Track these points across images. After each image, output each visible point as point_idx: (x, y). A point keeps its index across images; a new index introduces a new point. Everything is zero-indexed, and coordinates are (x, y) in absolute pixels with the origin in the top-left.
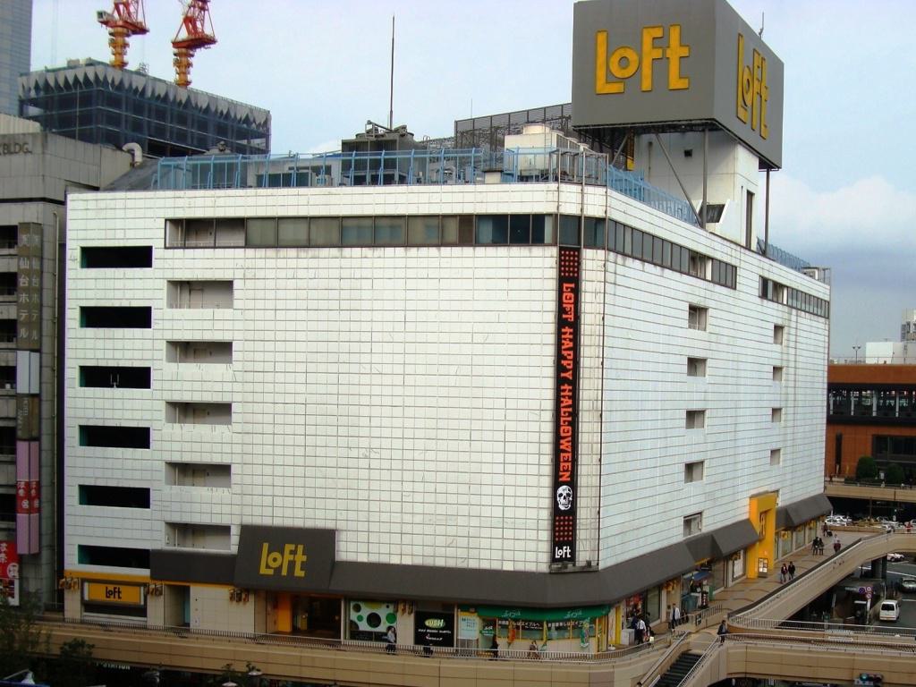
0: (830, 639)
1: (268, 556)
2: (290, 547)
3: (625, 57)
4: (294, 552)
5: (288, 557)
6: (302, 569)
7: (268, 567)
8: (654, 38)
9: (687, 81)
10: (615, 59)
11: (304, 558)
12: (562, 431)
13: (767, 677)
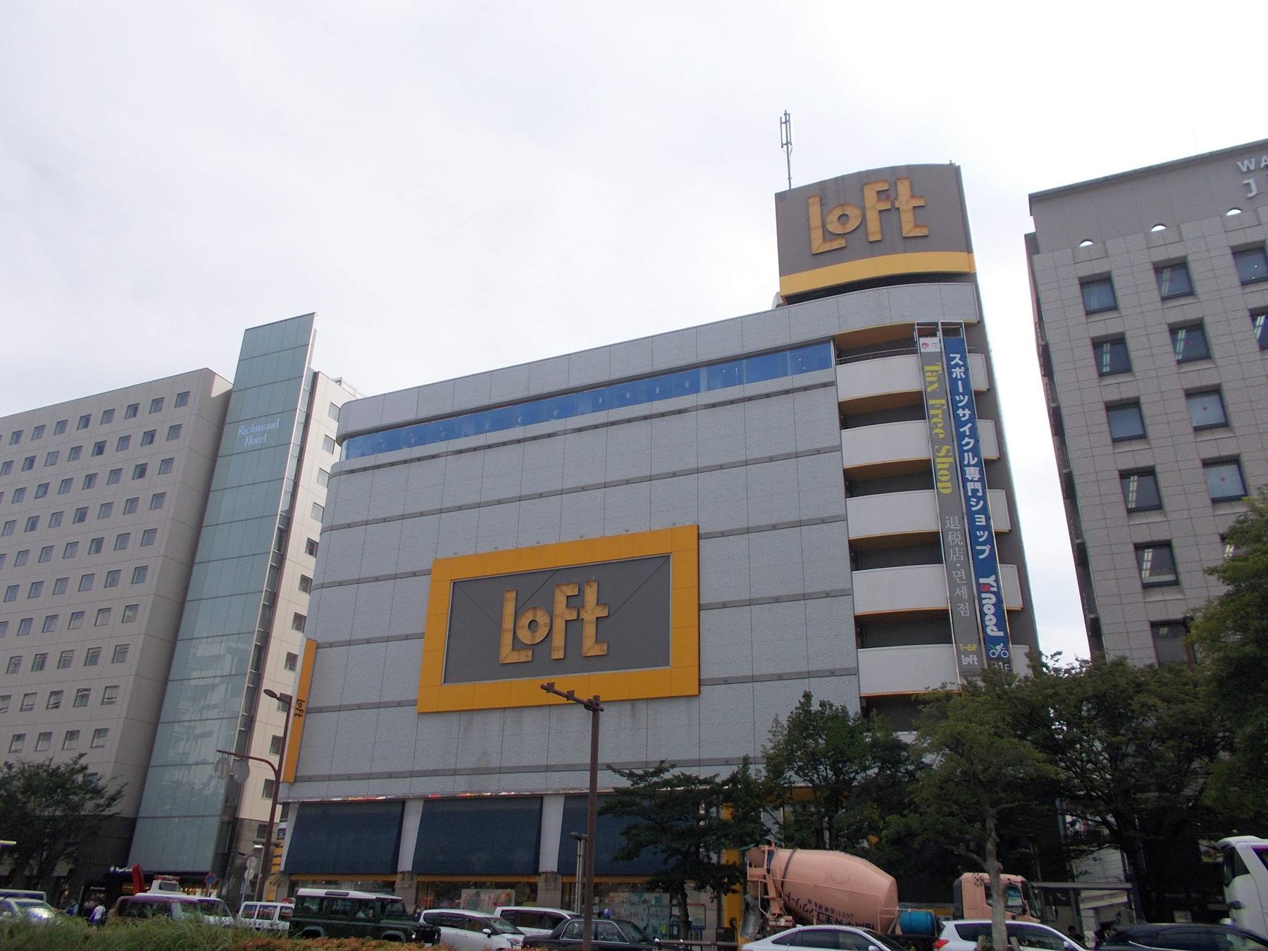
0: (171, 877)
2: (971, 656)
3: (847, 215)
4: (973, 657)
8: (880, 211)
9: (605, 647)
10: (525, 621)
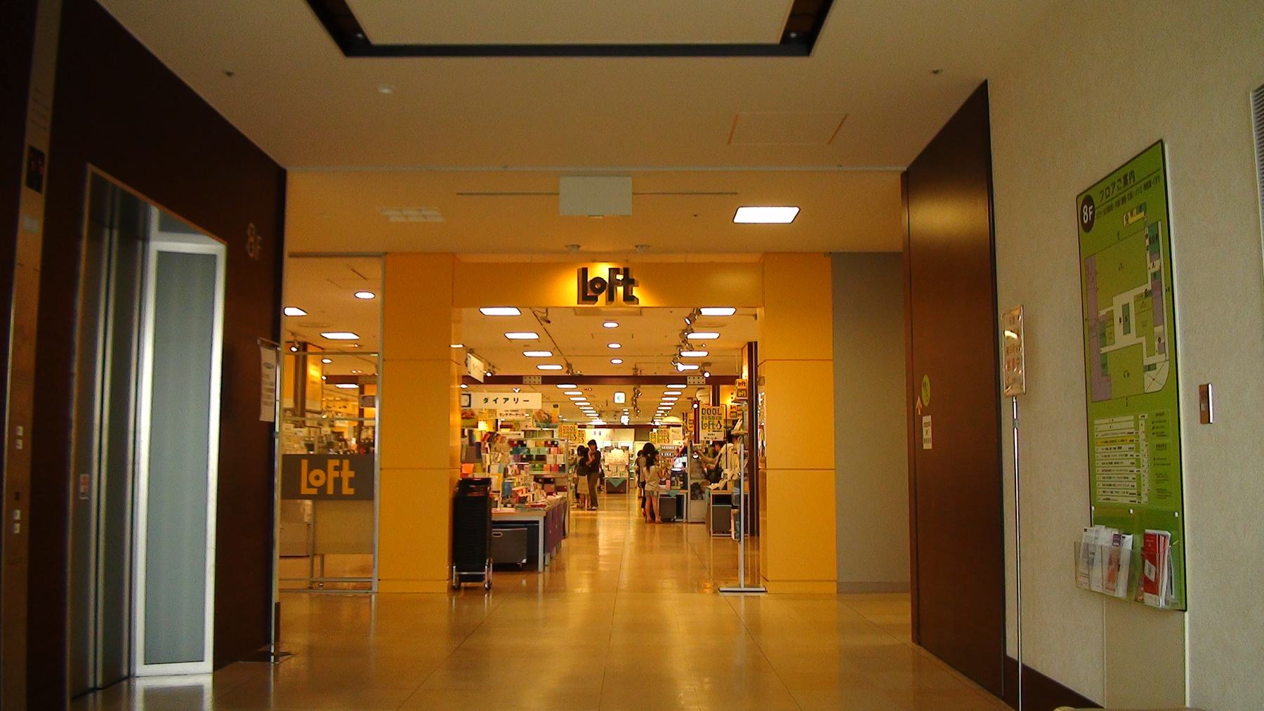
1: (1160, 267)
4: (338, 469)
5: (333, 474)
6: (350, 486)
7: (310, 486)
11: (352, 474)
12: (616, 398)
13: (1087, 193)
